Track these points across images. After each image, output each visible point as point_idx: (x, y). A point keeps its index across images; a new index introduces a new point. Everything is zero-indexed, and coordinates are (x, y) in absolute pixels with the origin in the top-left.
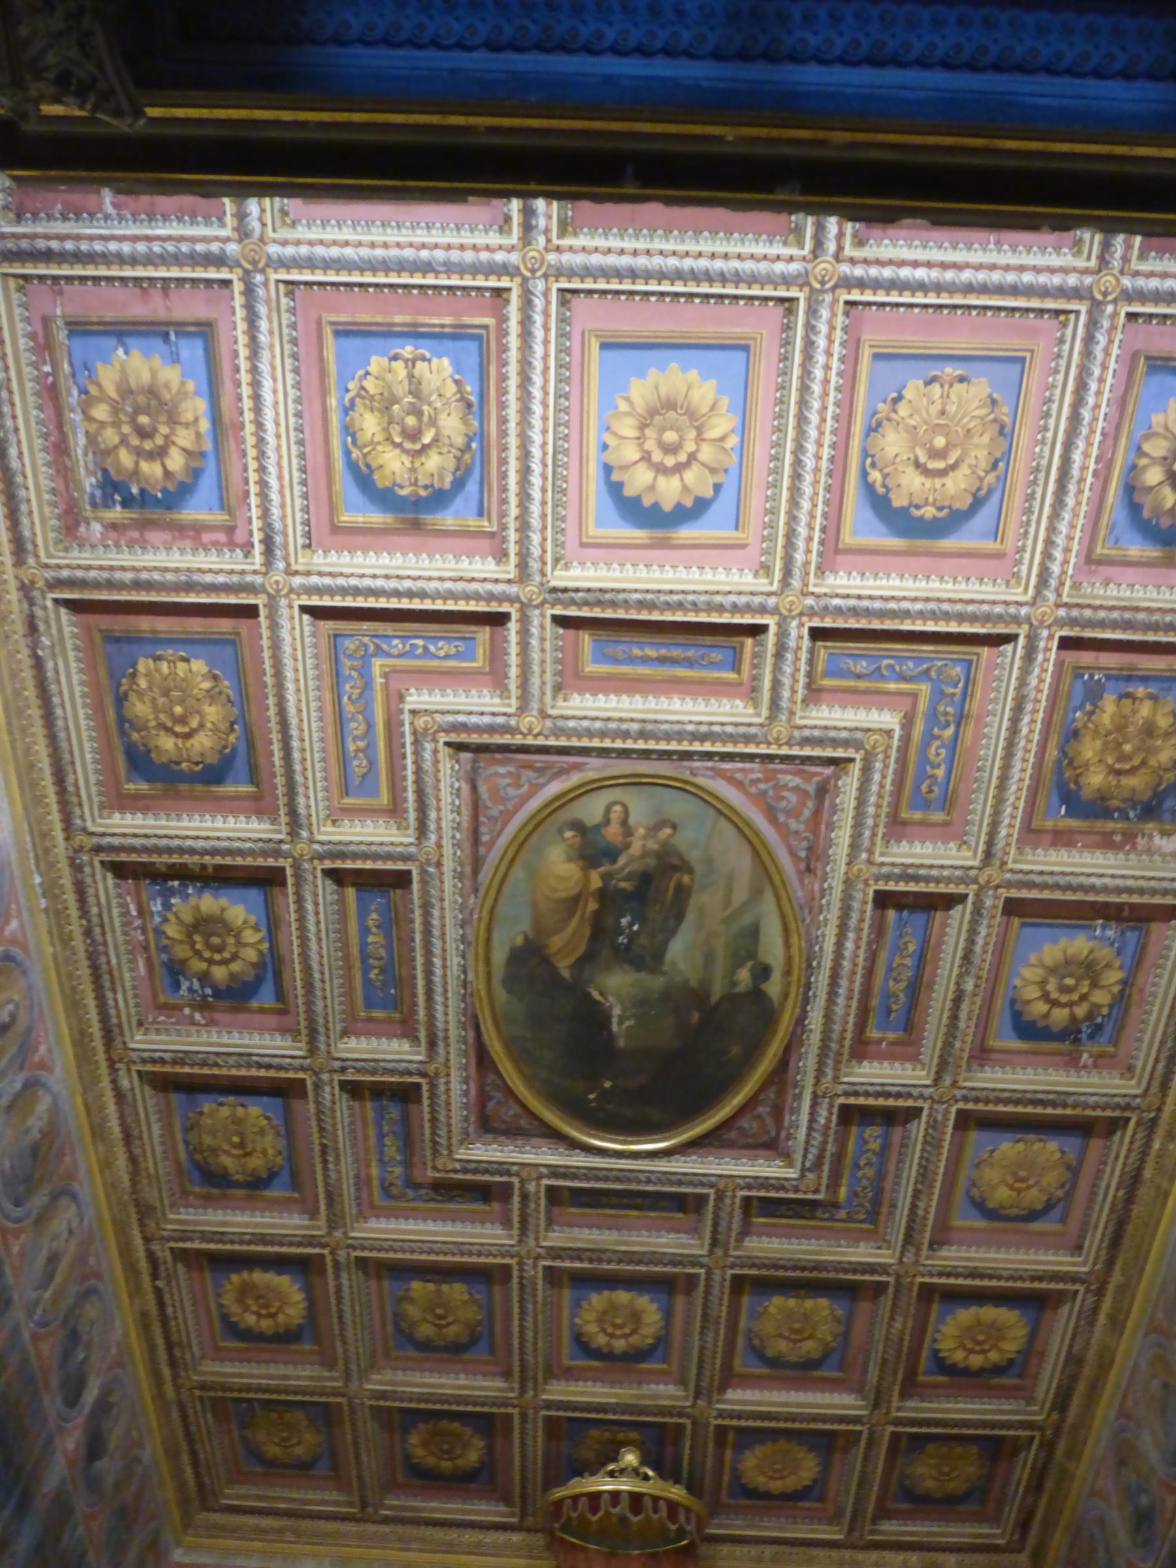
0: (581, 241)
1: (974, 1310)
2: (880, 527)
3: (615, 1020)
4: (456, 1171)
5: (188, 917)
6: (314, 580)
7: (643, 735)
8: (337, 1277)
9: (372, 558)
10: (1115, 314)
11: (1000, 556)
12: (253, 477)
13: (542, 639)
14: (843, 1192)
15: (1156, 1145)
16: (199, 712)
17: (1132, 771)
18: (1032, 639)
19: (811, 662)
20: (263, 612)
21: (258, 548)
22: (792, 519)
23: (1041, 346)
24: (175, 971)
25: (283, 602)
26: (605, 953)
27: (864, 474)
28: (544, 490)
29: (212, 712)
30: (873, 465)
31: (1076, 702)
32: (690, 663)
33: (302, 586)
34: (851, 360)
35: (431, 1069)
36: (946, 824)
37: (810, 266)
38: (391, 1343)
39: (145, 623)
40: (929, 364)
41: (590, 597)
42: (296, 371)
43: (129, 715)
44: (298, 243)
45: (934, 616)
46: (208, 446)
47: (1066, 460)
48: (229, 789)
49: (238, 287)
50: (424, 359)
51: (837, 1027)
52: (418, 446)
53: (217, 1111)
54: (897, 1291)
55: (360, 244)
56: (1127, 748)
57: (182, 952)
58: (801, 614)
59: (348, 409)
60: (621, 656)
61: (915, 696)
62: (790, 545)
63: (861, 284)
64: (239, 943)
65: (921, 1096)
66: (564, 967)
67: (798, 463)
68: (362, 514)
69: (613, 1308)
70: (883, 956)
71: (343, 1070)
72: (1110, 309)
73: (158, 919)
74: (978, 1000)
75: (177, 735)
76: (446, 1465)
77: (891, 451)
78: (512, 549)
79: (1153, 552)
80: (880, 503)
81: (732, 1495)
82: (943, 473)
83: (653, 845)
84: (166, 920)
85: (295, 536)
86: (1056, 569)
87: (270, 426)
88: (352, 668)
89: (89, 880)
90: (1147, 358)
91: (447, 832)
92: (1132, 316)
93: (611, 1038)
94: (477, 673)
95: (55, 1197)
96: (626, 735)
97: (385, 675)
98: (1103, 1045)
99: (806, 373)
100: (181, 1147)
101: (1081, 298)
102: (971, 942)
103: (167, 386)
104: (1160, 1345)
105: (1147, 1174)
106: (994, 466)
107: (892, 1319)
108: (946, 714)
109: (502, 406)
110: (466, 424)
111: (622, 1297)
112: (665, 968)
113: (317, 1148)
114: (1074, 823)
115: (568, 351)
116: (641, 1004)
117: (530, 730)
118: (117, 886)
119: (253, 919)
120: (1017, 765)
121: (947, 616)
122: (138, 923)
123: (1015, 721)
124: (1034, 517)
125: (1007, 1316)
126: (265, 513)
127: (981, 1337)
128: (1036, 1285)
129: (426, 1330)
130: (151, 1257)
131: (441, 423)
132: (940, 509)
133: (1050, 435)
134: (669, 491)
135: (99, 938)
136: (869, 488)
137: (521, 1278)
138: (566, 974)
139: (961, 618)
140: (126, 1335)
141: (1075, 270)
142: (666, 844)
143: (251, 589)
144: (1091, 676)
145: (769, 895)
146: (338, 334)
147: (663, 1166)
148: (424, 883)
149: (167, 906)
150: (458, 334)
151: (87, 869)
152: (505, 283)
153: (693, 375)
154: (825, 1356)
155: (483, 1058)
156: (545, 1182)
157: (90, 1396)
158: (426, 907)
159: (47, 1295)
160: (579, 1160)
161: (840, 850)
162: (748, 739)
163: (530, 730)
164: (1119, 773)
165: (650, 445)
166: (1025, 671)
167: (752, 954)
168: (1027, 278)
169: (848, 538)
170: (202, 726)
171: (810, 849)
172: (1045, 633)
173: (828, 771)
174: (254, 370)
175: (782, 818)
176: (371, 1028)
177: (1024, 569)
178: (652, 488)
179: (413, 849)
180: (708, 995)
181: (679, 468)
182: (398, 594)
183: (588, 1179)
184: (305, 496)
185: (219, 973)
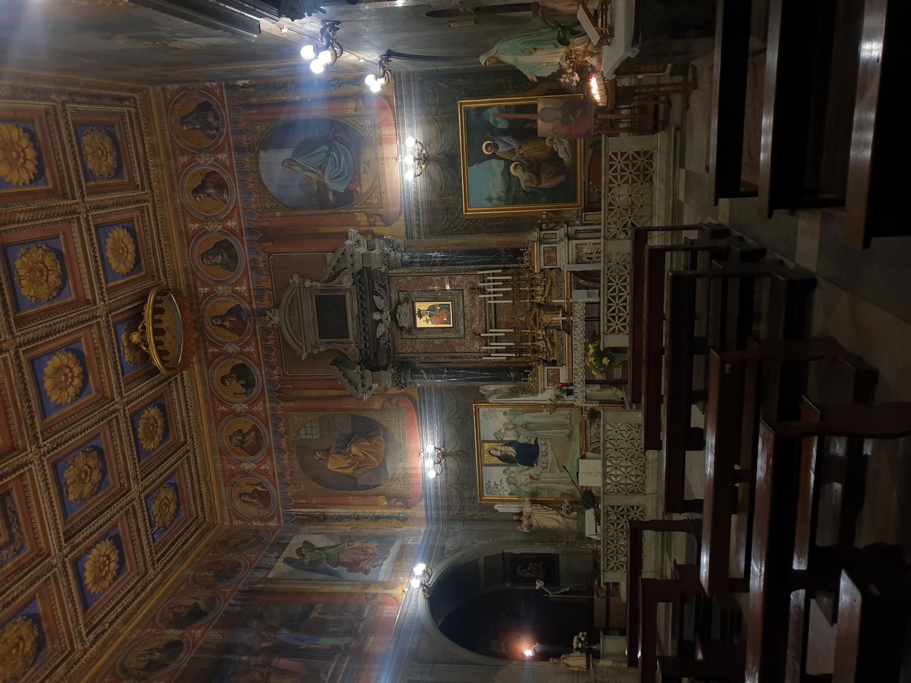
8: (80, 544)
69: (55, 386)
81: (141, 270)
107: (19, 222)
111: (48, 384)
127: (14, 155)
130: (93, 643)
140: (137, 626)
154: (52, 249)
157: (173, 634)
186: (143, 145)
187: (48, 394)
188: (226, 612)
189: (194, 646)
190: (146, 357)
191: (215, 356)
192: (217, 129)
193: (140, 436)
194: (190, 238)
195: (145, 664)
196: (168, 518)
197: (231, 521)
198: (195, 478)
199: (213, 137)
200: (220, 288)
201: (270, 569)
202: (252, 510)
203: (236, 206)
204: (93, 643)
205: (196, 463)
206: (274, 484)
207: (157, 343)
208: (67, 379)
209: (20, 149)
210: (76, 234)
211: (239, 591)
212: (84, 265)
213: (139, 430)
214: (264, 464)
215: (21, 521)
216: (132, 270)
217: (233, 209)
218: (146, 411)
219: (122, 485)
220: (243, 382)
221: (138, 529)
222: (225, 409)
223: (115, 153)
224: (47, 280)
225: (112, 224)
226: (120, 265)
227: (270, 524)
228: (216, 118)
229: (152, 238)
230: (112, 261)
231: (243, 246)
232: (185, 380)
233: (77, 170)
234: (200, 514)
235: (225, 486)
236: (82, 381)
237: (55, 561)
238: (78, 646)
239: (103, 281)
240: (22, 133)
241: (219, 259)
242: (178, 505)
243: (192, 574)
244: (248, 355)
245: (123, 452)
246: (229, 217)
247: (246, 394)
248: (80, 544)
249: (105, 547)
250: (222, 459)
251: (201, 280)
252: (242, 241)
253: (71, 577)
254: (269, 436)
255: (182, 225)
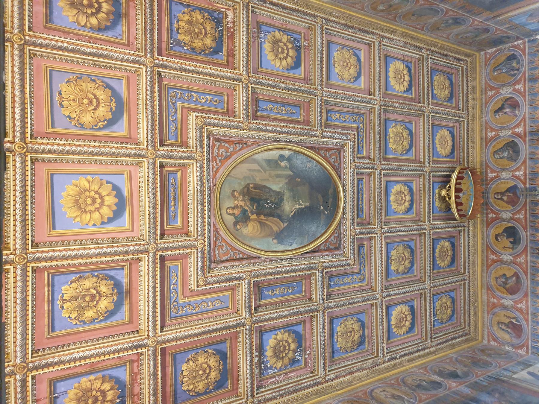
0: (11, 243)
1: (390, 79)
2: (120, 122)
3: (300, 207)
4: (354, 257)
5: (274, 360)
6: (150, 328)
7: (202, 204)
8: (392, 295)
9: (141, 307)
10: (29, 35)
11: (128, 78)
12: (112, 356)
13: (169, 242)
14: (354, 126)
15: (334, 19)
16: (201, 365)
17: (205, 28)
18: (159, 66)
19: (172, 146)
20: (163, 346)
21: (140, 351)
22: (119, 155)
23: (45, 63)
24: (293, 362)
25: (159, 339)
26: (279, 212)
27: (100, 129)
28: (113, 247)
29: (201, 360)
30: (96, 126)
31: (181, 49)
32: (175, 189)
33: (153, 332)
34: (55, 136)
35: (321, 268)
36: (227, 95)
37: (17, 153)
38: (412, 275)
39: (170, 389)
40: (55, 106)
41: (152, 226)
42: (69, 345)
43: (204, 390)
44: (15, 351)
45: (153, 101)
46: (100, 375)
47: (90, 54)
48: (228, 350)
49: (35, 373)
50: (63, 296)
51: (299, 131)
52: (97, 295)
53: (340, 342)
54: (386, 106)
55: (15, 327)
56: (197, 30)
57: (286, 360)
58: (155, 150)
59: (84, 323)
60: (174, 213)
61: (182, 108)
62: (129, 155)
63: (23, 133)
64: (282, 340)
65: (321, 100)
66: (283, 225)
67: (97, 154)
68: (124, 314)
70: (274, 116)
71: (323, 299)
72: (27, 38)
73: (276, 371)
74: (288, 82)
75: (210, 372)
76: (450, 253)
77: (90, 119)
78: (136, 256)
79: (123, 21)
80: (111, 123)
81: (453, 158)
82: (98, 100)
83: (241, 198)
84: (276, 368)
85: (134, 339)
86: (132, 57)
87: (91, 352)
88: (182, 310)
89: (263, 398)
90: (46, 23)
91: (240, 270)
92: (30, 29)
93: (306, 207)
94: (182, 264)
95: (373, 398)
96: (203, 210)
97: (185, 297)
98: (301, 38)
99: (61, 152)
100: (352, 354)
101: (24, 48)
102: (268, 85)
103: (76, 394)
104: (400, 17)
105: (344, 22)
106: (94, 81)
107: (395, 107)
108: (188, 96)
109: (80, 265)
110: (88, 278)
111: (392, 198)
112: (282, 191)
113: (350, 306)
114: (225, 49)
115: (57, 242)
116: (295, 198)
117: (202, 244)
118: (265, 387)
119: (273, 336)
120: (205, 70)
121: (152, 97)
122: (277, 378)
123: (189, 71)
124: (113, 66)
125: (391, 69)
126: (126, 349)
127: (399, 77)
128: (382, 59)
129: (407, 263)
130: (389, 361)
131: (88, 287)
132: (112, 100)
133: (80, 60)
134: (110, 200)
135: (283, 391)
136: (105, 127)
137: (388, 233)
138: (286, 224)
139: (152, 92)
140: (416, 367)
141: (12, 51)
142: (240, 194)
143: (155, 351)
144: (171, 44)
145: (256, 157)
146: (53, 331)
147: (348, 187)
148: (258, 276)
149: (271, 368)
150: (51, 284)
151: (260, 399)
152: (30, 269)
153: (64, 194)
154: (408, 129)
155: (316, 251)
156: (356, 227)
157: (437, 378)
158: (266, 274)
159: (406, 398)
160: (348, 216)
161: (239, 132)
162: (202, 167)
163: (202, 244)
164: (206, 33)
165: (93, 208)
166: (171, 68)
167: (276, 162)
168: (16, 69)
169: (125, 134)
170: (206, 363)
171: (239, 144)
172: (156, 61)
173: (211, 138)
174: (69, 362)
175: (229, 154)
176: (308, 290)
177: (132, 69)
178: (109, 206)
179: (246, 282)
180: (290, 176)
181: (101, 197)
182: (155, 297)
183: (354, 212)
184: (119, 335)
185: (293, 346)
186: (468, 87)
187: (391, 203)
188: (476, 382)
189: (449, 389)
190: (448, 208)
191: (493, 220)
192: (518, 70)
193: (437, 255)
194: (487, 141)
195: (416, 384)
196: (445, 316)
197: (489, 341)
198: (467, 301)
199: (514, 75)
200: (504, 173)
201: (515, 373)
202: (507, 337)
203: (524, 118)
204: (389, 361)
205: (469, 292)
206: (527, 321)
207: (457, 197)
208: (402, 200)
209: (402, 75)
210: (421, 124)
211: (488, 376)
212: (422, 142)
213: (437, 250)
214: (521, 303)
215: (366, 265)
216: (448, 155)
217: (522, 120)
218: (442, 242)
219: (421, 278)
220: (511, 239)
221: (426, 310)
222: (495, 258)
223: (450, 89)
224: (402, 143)
225: (442, 126)
226: (443, 150)
227: (520, 351)
228: (518, 63)
229: (464, 140)
230: (438, 146)
231: (525, 144)
232: (470, 233)
233: (428, 90)
234: (467, 327)
235: (488, 313)
236: (410, 205)
237: (378, 296)
238: (381, 355)
239: (431, 155)
240: (405, 67)
241: (506, 154)
242: (453, 311)
243: (456, 357)
244: (518, 220)
245: (425, 257)
246: (518, 126)
247: (513, 248)
248: (392, 295)
249: (404, 309)
250: (487, 293)
251: (491, 169)
252: (525, 141)
253: (385, 331)
254: (527, 282)
255: (484, 135)
